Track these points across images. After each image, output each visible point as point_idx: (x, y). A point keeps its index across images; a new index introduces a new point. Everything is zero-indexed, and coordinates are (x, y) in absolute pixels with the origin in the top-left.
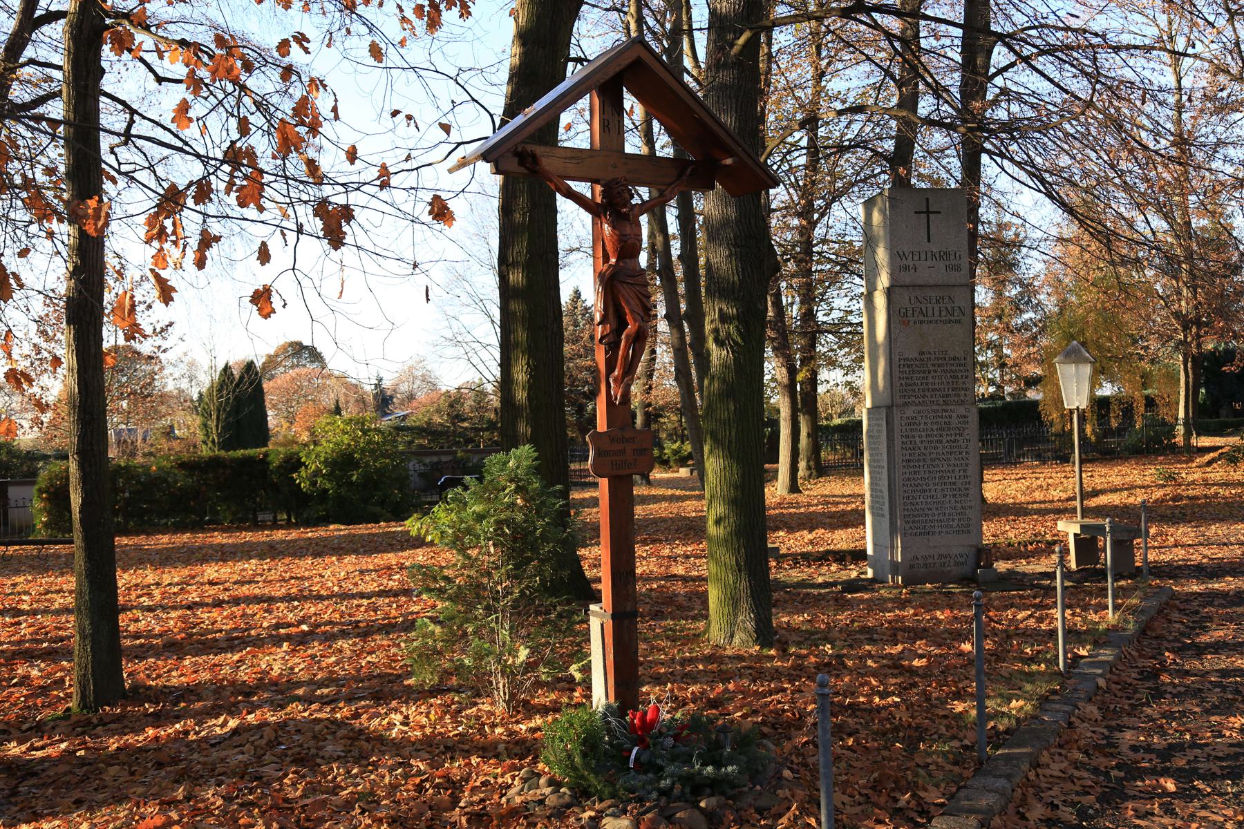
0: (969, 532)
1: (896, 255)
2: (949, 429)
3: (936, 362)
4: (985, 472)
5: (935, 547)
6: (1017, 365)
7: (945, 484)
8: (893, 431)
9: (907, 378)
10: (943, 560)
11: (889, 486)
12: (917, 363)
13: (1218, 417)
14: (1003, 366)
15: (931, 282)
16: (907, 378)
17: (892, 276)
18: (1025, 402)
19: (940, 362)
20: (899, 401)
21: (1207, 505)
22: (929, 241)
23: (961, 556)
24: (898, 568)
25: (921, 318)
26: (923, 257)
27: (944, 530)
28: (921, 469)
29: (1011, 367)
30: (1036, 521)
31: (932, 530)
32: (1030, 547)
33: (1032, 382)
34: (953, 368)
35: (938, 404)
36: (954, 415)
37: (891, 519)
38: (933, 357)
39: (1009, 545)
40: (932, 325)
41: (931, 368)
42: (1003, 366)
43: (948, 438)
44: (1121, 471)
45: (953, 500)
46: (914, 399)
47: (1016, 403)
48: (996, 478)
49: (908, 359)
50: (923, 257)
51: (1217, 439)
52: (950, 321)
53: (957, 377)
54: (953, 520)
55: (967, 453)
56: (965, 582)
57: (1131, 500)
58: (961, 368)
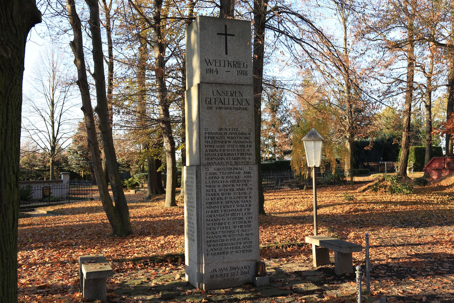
0: (251, 251)
1: (204, 62)
2: (238, 182)
3: (230, 135)
4: (266, 196)
5: (228, 262)
6: (281, 146)
7: (235, 219)
8: (200, 183)
9: (211, 146)
10: (234, 271)
11: (197, 220)
12: (217, 136)
13: (358, 168)
14: (275, 146)
15: (228, 82)
16: (211, 146)
17: (202, 77)
18: (284, 161)
19: (233, 136)
20: (204, 162)
21: (371, 214)
22: (226, 54)
23: (246, 267)
24: (202, 278)
25: (221, 105)
26: (222, 64)
27: (234, 250)
28: (219, 209)
29: (278, 146)
30: (291, 228)
31: (226, 250)
32: (288, 249)
33: (287, 153)
34: (242, 140)
35: (231, 164)
36: (242, 172)
37: (198, 244)
38: (228, 132)
39: (277, 248)
40: (228, 111)
41: (227, 140)
42: (275, 146)
43: (238, 187)
44: (327, 194)
45: (240, 229)
46: (215, 160)
47: (280, 161)
48: (271, 198)
49: (211, 133)
50: (222, 64)
51: (360, 178)
52: (240, 108)
53: (244, 146)
54: (240, 243)
55: (250, 197)
56: (248, 286)
57: (335, 211)
58: (247, 140)
